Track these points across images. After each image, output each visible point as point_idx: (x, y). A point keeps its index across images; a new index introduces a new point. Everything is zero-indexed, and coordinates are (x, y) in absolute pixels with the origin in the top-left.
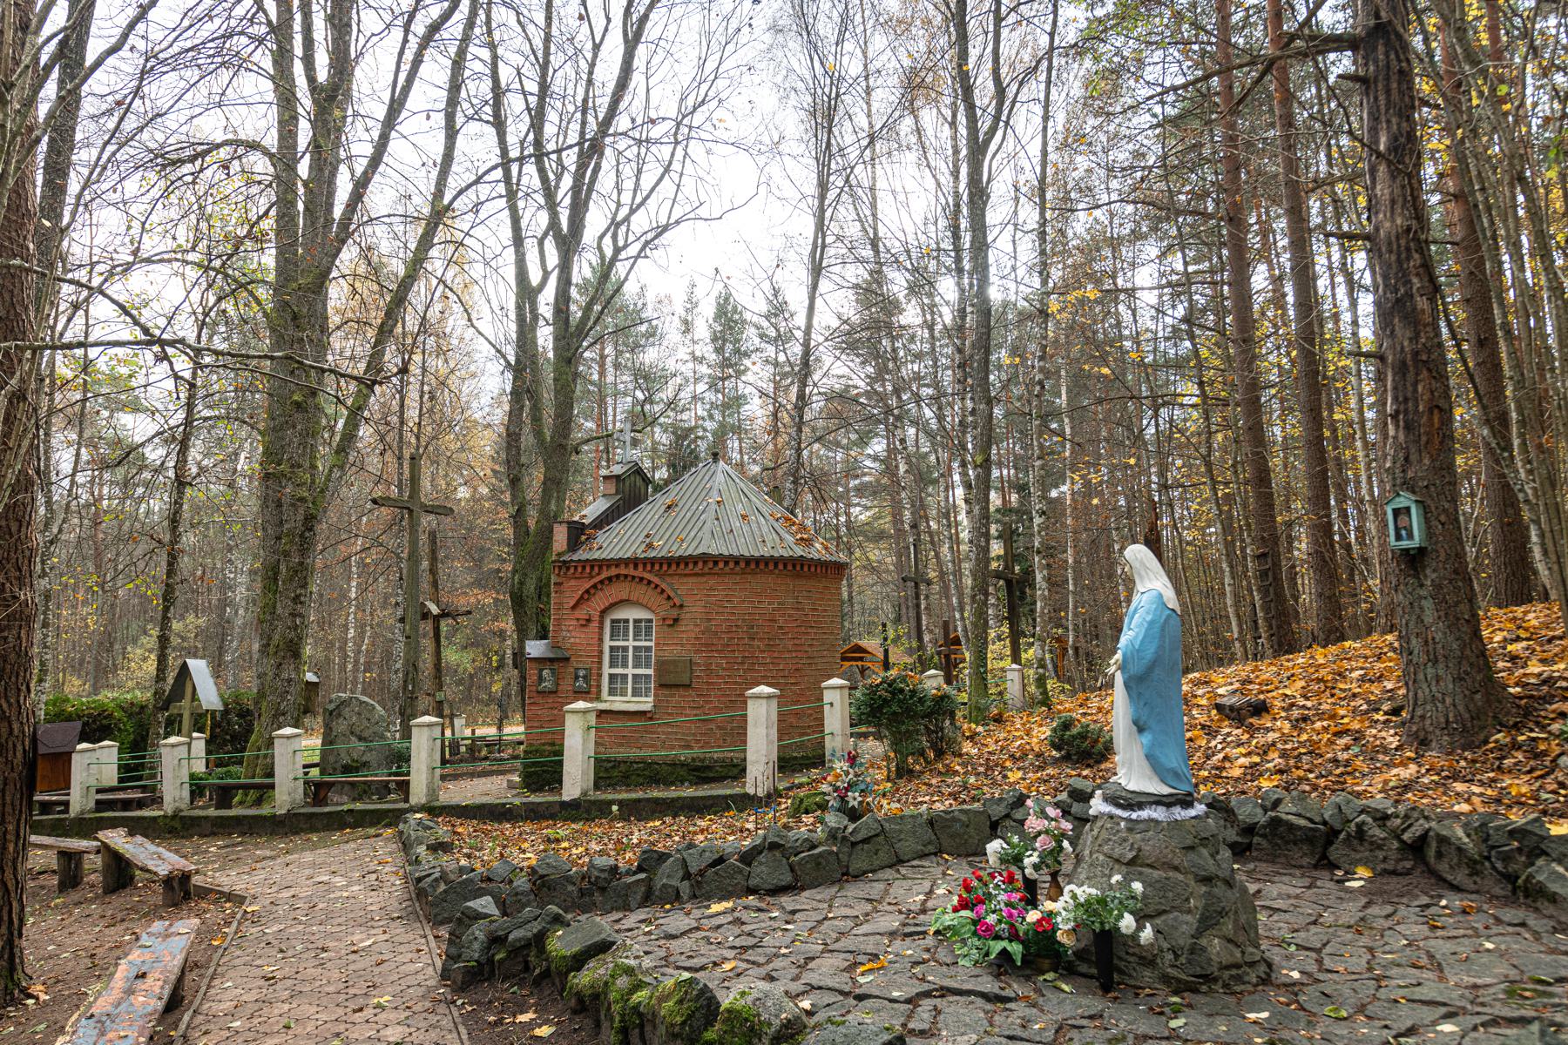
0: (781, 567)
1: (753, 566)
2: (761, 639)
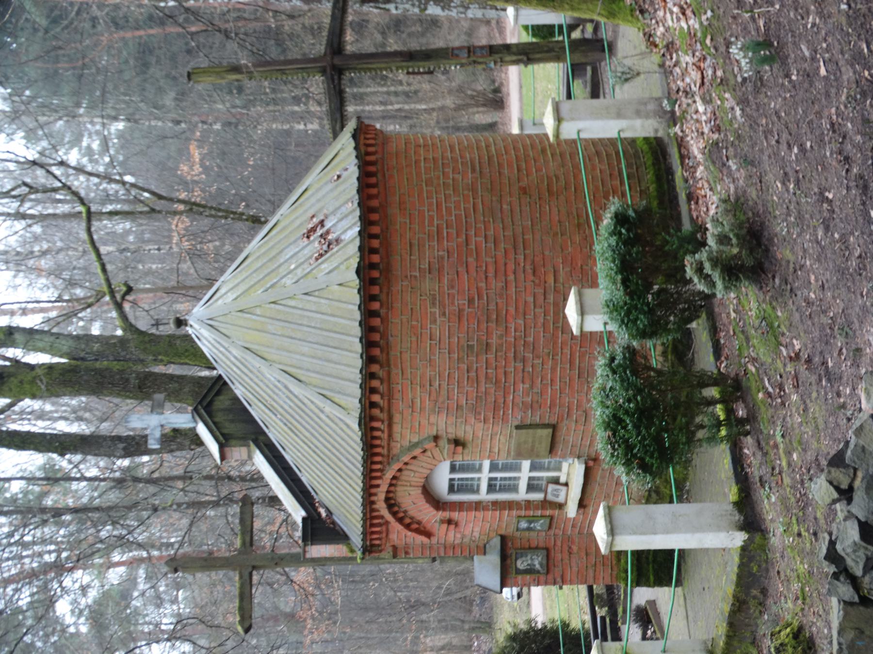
0: (376, 306)
1: (376, 352)
2: (488, 333)
